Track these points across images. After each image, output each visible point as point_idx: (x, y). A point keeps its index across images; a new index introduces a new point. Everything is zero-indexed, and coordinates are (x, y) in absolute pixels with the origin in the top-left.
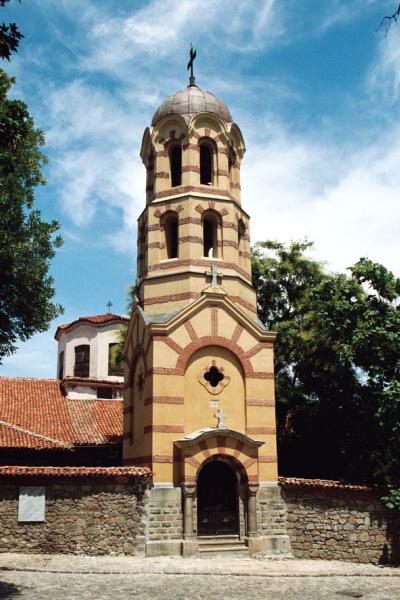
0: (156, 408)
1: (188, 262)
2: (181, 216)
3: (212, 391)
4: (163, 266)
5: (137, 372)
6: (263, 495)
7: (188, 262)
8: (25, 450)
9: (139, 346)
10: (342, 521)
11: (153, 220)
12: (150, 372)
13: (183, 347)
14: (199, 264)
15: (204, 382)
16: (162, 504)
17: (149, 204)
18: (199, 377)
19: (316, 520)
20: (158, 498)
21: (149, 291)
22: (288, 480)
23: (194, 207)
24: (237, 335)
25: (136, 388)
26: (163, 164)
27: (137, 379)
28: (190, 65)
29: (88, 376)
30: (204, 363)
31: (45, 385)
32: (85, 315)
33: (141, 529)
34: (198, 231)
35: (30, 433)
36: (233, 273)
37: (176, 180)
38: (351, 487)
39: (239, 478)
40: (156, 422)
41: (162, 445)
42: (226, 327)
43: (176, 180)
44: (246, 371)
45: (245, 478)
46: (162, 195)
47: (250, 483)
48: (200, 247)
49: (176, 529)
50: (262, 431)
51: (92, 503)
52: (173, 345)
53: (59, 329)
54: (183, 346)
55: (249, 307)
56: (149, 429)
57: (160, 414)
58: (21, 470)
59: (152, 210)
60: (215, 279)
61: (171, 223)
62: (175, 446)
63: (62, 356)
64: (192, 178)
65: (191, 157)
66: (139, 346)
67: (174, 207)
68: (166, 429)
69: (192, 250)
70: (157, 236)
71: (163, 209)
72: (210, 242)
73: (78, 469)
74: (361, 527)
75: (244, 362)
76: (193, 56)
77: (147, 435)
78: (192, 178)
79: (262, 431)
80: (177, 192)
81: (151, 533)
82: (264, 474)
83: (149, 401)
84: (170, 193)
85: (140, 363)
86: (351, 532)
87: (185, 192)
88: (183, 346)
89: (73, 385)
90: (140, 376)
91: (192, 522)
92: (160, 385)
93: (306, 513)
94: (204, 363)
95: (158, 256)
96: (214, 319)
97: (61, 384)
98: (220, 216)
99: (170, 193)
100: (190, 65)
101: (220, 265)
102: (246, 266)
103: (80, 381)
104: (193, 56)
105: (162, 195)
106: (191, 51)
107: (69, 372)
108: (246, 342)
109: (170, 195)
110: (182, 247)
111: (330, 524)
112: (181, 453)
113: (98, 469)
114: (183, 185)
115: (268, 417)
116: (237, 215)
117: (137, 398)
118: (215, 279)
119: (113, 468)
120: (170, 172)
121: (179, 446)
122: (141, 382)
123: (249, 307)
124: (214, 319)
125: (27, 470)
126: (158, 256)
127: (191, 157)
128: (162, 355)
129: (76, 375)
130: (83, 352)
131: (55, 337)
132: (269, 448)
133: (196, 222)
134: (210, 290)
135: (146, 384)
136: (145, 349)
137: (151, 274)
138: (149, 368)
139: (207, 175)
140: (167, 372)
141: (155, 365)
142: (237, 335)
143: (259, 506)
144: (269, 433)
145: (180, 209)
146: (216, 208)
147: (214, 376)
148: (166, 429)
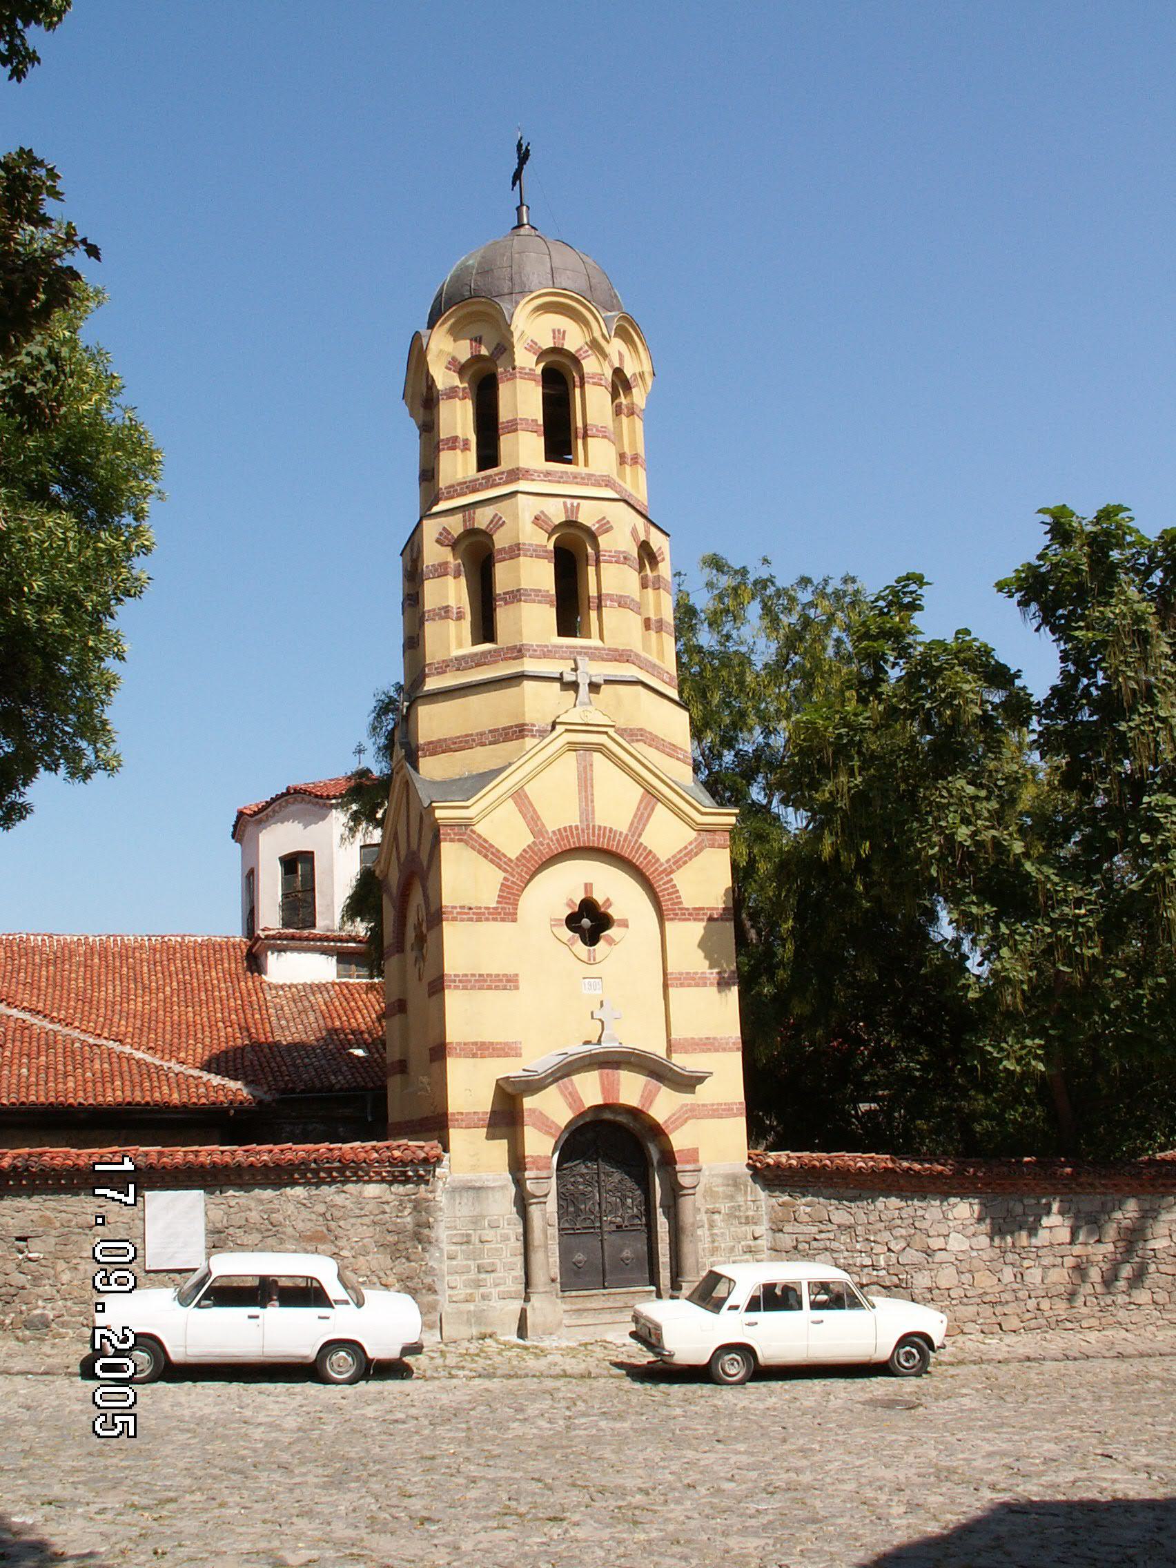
0: (454, 1001)
1: (518, 652)
2: (501, 540)
3: (584, 957)
4: (462, 664)
5: (412, 920)
6: (710, 1193)
7: (518, 652)
8: (166, 1107)
9: (413, 856)
10: (895, 1246)
11: (433, 553)
12: (435, 917)
13: (506, 1141)
14: (547, 653)
15: (567, 934)
16: (476, 1221)
17: (425, 515)
18: (554, 923)
19: (834, 1245)
20: (464, 1208)
21: (432, 721)
22: (772, 1157)
23: (526, 518)
24: (641, 819)
25: (411, 955)
26: (458, 418)
27: (411, 935)
28: (517, 176)
29: (313, 925)
30: (565, 885)
31: (212, 950)
32: (299, 781)
33: (428, 1280)
34: (540, 575)
35: (178, 1068)
36: (630, 671)
37: (488, 456)
38: (917, 1167)
39: (655, 1155)
40: (454, 1034)
41: (468, 1087)
42: (616, 801)
43: (488, 456)
44: (666, 905)
45: (669, 1159)
46: (453, 492)
47: (678, 1167)
48: (549, 614)
49: (512, 1277)
50: (708, 1045)
51: (310, 1224)
52: (488, 851)
53: (241, 814)
54: (513, 852)
55: (670, 750)
56: (439, 1052)
57: (461, 1016)
58: (146, 1154)
59: (431, 529)
60: (583, 688)
61: (479, 557)
62: (497, 1084)
63: (250, 877)
64: (525, 447)
65: (523, 400)
66: (413, 856)
67: (482, 519)
68: (481, 1050)
69: (531, 621)
70: (449, 592)
71: (456, 525)
72: (571, 609)
73: (277, 1148)
74: (939, 1256)
75: (659, 885)
76: (524, 157)
77: (436, 1065)
78: (525, 447)
79: (708, 1045)
80: (490, 483)
81: (451, 1258)
82: (712, 1136)
83: (437, 986)
84: (473, 487)
85: (417, 898)
86: (918, 1267)
87: (507, 483)
88: (513, 852)
89: (282, 944)
90: (418, 926)
91: (548, 1261)
92: (460, 948)
93: (815, 1229)
94: (565, 885)
95: (450, 639)
96: (585, 782)
97: (251, 947)
98: (593, 537)
99: (473, 487)
100: (517, 176)
101: (594, 655)
102: (661, 653)
103: (293, 938)
104: (524, 157)
105: (453, 492)
106: (519, 146)
107: (270, 918)
108: (665, 836)
109: (475, 490)
110: (503, 615)
111: (870, 1253)
112: (506, 1115)
113: (323, 1147)
114: (505, 465)
115: (716, 1014)
116: (634, 532)
117: (412, 972)
118: (583, 688)
119: (357, 1144)
120: (473, 439)
121: (509, 1090)
122: (421, 939)
123: (670, 750)
124: (585, 782)
125: (161, 1154)
126: (450, 639)
127: (523, 400)
128: (461, 877)
129: (286, 925)
130: (297, 866)
131: (233, 837)
132: (726, 1079)
133: (538, 553)
134: (574, 716)
135: (431, 937)
136: (425, 864)
137: (431, 684)
138: (433, 909)
139: (560, 439)
140: (477, 915)
141: (447, 900)
142: (641, 819)
143: (703, 1217)
144: (731, 1050)
145: (497, 523)
146: (582, 519)
147: (590, 922)
148: (481, 1050)
